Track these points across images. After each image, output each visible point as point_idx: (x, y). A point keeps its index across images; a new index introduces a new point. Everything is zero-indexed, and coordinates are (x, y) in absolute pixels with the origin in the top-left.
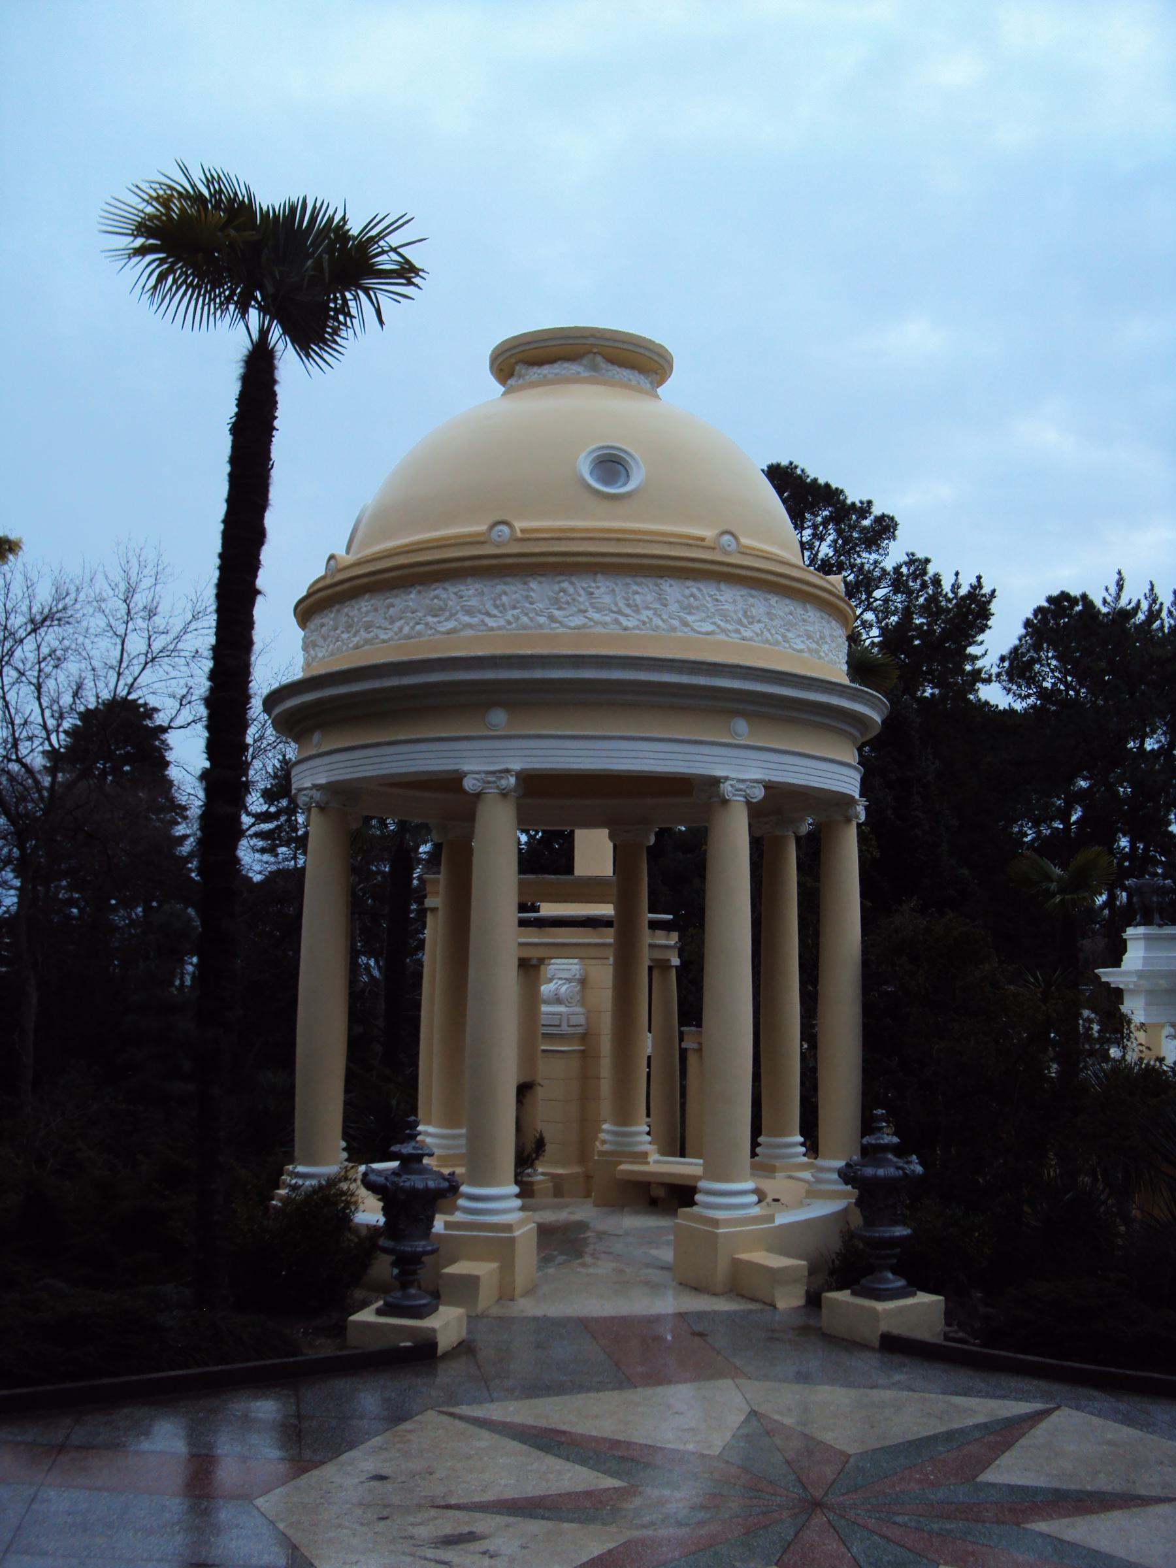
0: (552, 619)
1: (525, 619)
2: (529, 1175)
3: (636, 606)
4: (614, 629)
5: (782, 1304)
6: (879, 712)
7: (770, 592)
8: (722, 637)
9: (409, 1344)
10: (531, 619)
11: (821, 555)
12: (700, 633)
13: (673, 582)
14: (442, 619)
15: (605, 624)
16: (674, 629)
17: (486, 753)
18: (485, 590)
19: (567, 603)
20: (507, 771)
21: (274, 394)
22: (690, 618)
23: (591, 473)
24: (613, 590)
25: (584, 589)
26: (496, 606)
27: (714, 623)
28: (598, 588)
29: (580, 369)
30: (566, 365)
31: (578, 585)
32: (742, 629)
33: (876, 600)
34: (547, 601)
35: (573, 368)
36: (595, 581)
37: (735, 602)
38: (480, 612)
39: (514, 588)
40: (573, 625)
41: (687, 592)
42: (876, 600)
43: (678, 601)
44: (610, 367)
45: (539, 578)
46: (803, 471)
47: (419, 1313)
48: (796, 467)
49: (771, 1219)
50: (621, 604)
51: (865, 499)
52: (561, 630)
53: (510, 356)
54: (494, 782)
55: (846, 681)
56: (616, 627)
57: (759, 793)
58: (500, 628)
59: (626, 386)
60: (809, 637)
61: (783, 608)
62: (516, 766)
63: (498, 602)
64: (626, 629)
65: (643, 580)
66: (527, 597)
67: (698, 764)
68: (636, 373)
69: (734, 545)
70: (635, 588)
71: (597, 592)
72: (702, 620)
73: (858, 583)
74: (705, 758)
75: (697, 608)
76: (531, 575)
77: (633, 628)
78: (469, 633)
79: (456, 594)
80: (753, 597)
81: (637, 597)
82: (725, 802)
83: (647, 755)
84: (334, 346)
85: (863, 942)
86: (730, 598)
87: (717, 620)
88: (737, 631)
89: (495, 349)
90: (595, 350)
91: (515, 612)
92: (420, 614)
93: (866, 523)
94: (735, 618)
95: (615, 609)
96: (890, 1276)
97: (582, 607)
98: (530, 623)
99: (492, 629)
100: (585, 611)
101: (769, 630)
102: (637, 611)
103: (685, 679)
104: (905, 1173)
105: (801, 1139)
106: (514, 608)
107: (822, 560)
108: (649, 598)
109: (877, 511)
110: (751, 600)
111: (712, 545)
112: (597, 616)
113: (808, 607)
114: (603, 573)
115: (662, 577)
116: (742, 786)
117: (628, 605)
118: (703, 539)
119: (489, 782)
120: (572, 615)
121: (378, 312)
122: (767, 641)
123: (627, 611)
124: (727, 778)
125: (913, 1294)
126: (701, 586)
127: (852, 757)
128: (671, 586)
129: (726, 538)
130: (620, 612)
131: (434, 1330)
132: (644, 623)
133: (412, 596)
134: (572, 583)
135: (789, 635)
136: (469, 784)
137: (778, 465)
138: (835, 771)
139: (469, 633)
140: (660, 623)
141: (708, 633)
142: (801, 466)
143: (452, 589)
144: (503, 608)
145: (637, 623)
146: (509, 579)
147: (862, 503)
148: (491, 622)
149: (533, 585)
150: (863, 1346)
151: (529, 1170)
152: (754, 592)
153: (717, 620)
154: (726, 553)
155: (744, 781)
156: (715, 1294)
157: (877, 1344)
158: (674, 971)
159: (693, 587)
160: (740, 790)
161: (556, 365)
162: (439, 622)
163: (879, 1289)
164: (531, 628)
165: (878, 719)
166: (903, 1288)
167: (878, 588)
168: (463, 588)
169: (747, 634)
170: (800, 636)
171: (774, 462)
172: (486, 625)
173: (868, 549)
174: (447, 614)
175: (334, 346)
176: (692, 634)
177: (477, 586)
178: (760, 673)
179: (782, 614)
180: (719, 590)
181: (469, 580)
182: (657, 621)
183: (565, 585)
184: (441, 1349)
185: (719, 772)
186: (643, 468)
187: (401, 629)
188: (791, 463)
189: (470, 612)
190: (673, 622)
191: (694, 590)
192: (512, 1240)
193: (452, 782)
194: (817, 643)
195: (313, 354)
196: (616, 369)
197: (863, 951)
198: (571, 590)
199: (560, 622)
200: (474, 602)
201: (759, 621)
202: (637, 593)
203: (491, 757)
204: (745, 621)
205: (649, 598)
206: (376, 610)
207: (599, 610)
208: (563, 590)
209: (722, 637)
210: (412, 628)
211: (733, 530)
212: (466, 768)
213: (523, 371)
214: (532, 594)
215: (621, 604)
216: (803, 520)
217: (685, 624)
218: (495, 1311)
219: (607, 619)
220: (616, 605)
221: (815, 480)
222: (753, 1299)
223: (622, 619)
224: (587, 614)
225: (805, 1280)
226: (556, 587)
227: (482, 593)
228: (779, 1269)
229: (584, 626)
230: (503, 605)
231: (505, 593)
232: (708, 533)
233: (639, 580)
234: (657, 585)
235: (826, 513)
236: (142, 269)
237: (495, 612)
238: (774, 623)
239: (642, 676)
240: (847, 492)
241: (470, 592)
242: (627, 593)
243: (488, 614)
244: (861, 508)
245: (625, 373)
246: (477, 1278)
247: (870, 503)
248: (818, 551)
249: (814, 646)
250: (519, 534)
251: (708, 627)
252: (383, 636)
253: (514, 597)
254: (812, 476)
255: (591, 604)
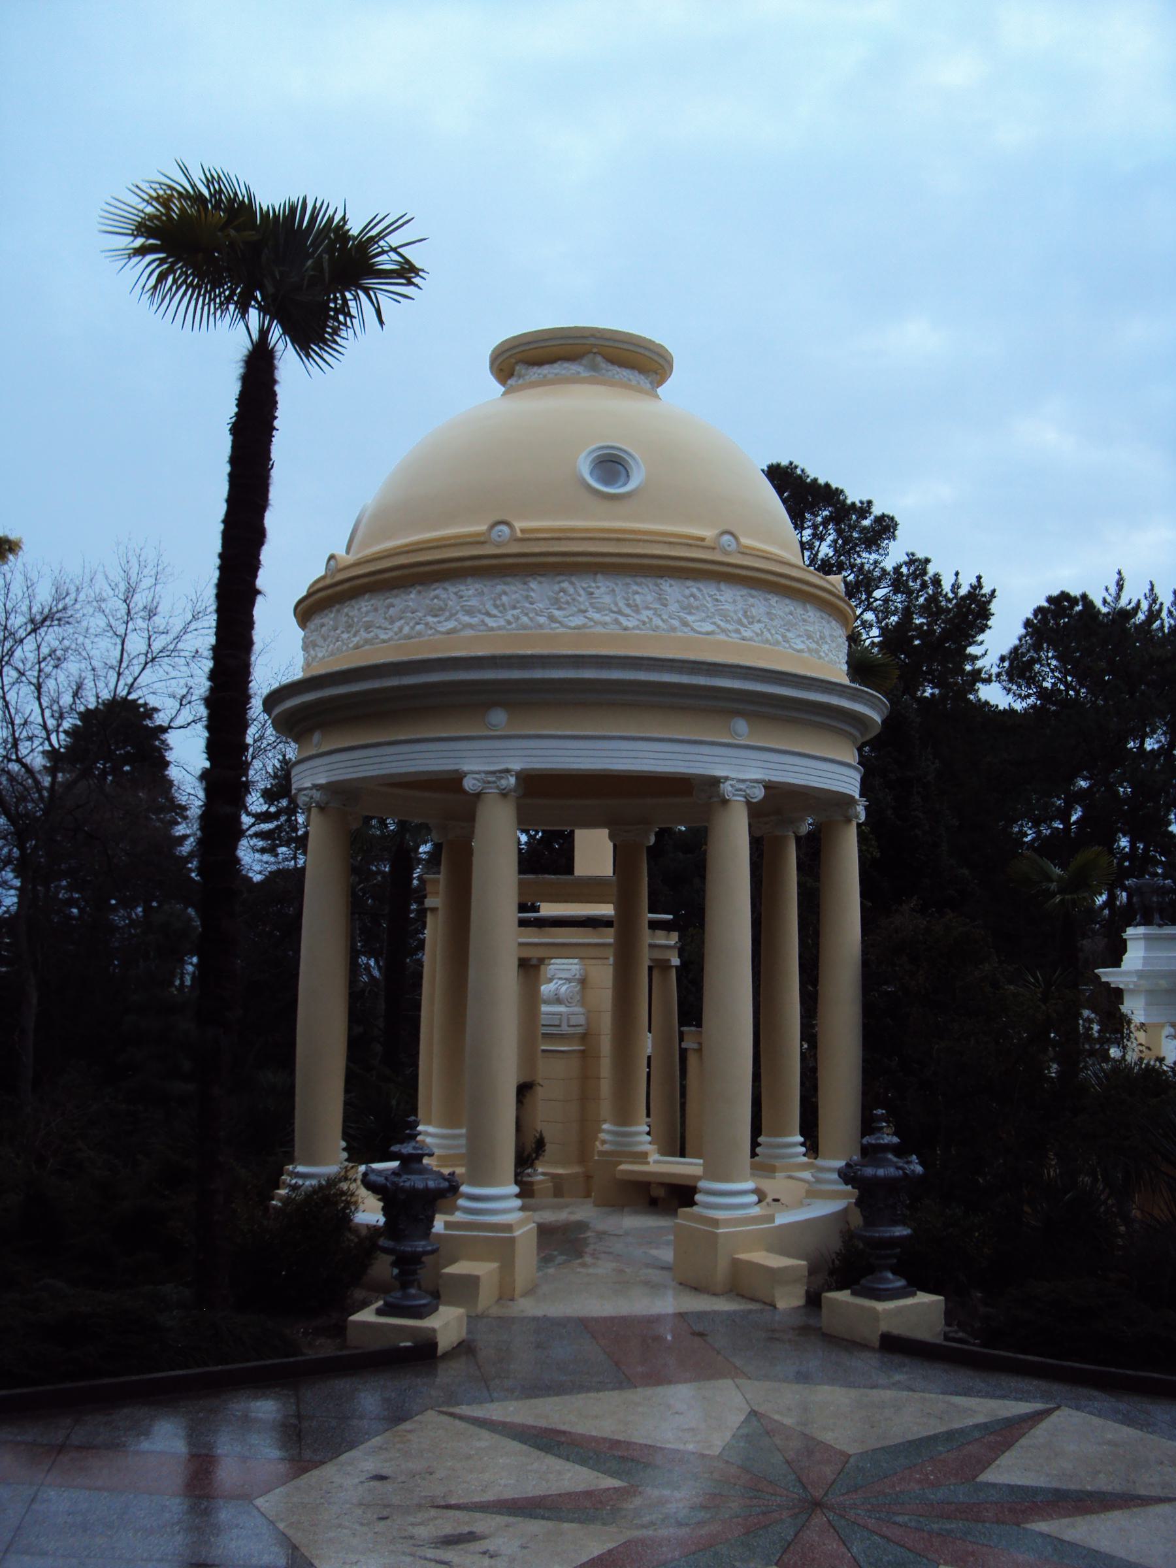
0: (552, 619)
1: (525, 619)
2: (529, 1175)
3: (636, 606)
4: (614, 629)
5: (782, 1304)
6: (879, 712)
7: (770, 592)
8: (722, 637)
9: (409, 1344)
10: (531, 619)
11: (821, 555)
12: (700, 633)
13: (673, 582)
14: (442, 619)
15: (605, 624)
16: (674, 629)
17: (486, 753)
18: (485, 590)
19: (567, 603)
20: (507, 771)
21: (274, 394)
22: (690, 618)
23: (591, 473)
24: (613, 590)
25: (584, 589)
26: (496, 606)
27: (714, 623)
28: (598, 588)
29: (580, 369)
30: (566, 365)
31: (578, 585)
32: (742, 629)
33: (876, 600)
34: (547, 601)
35: (573, 368)
36: (595, 581)
37: (735, 602)
38: (480, 612)
39: (514, 588)
40: (573, 625)
41: (687, 592)
42: (876, 600)
43: (678, 601)
44: (610, 367)
45: (539, 578)
46: (803, 471)
47: (419, 1313)
48: (796, 467)
49: (771, 1219)
50: (621, 604)
51: (865, 499)
52: (561, 630)
53: (510, 356)
54: (494, 782)
55: (846, 681)
56: (616, 627)
57: (759, 793)
58: (500, 628)
59: (626, 386)
60: (809, 637)
61: (783, 608)
62: (516, 766)
63: (498, 602)
64: (626, 629)
65: (643, 580)
66: (527, 597)
67: (698, 764)
68: (636, 373)
69: (734, 545)
70: (635, 588)
71: (597, 592)
72: (702, 620)
73: (858, 583)
74: (705, 758)
75: (697, 608)
76: (531, 575)
77: (633, 628)
78: (469, 633)
79: (456, 594)
80: (753, 597)
81: (637, 597)
82: (725, 802)
83: (647, 755)
84: (334, 346)
85: (863, 942)
86: (730, 598)
87: (717, 620)
88: (737, 631)
89: (495, 349)
90: (595, 350)
91: (515, 612)
92: (420, 614)
93: (866, 523)
94: (735, 618)
95: (615, 609)
96: (890, 1276)
97: (582, 607)
98: (530, 623)
99: (492, 629)
100: (585, 611)
101: (769, 630)
102: (637, 611)
103: (685, 679)
104: (905, 1173)
105: (801, 1139)
106: (514, 608)
107: (822, 560)
108: (649, 598)
109: (877, 511)
110: (751, 600)
111: (712, 545)
112: (597, 616)
113: (808, 607)
114: (603, 573)
115: (662, 577)
116: (742, 786)
117: (628, 605)
118: (703, 539)
119: (489, 782)
120: (572, 615)
121: (378, 312)
122: (767, 641)
123: (627, 611)
124: (727, 778)
125: (913, 1294)
126: (701, 586)
127: (852, 757)
128: (671, 586)
129: (726, 538)
130: (620, 612)
131: (434, 1330)
132: (644, 623)
133: (412, 596)
134: (572, 583)
135: (789, 635)
136: (469, 784)
137: (778, 465)
138: (835, 771)
139: (469, 633)
140: (660, 623)
141: (708, 633)
142: (801, 466)
143: (452, 589)
144: (503, 608)
145: (637, 623)
146: (509, 579)
147: (862, 503)
148: (491, 622)
149: (533, 585)
150: (863, 1346)
151: (529, 1170)
152: (754, 592)
153: (717, 620)
154: (726, 553)
155: (744, 781)
156: (715, 1294)
157: (877, 1344)
158: (674, 971)
159: (693, 587)
160: (740, 790)
161: (556, 365)
162: (439, 622)
163: (879, 1289)
164: (531, 628)
165: (878, 719)
166: (903, 1288)
167: (878, 588)
168: (463, 588)
169: (747, 634)
170: (800, 636)
171: (774, 462)
172: (486, 625)
173: (868, 549)
174: (447, 614)
175: (334, 346)
176: (692, 634)
177: (477, 586)
178: (760, 673)
179: (782, 614)
180: (719, 590)
181: (469, 580)
182: (657, 621)
183: (565, 585)
184: (441, 1349)
185: (719, 772)
186: (643, 468)
187: (401, 629)
188: (791, 463)
189: (470, 612)
190: (673, 622)
191: (694, 590)
192: (512, 1240)
193: (452, 782)
194: (817, 643)
195: (313, 354)
196: (616, 369)
197: (863, 951)
198: (571, 590)
199: (560, 622)
200: (474, 602)
201: (759, 621)
202: (637, 593)
203: (491, 757)
204: (745, 621)
205: (649, 598)
206: (376, 610)
207: (599, 610)
208: (563, 590)
209: (722, 637)
210: (412, 628)
211: (733, 530)
212: (466, 768)
213: (523, 371)
214: (532, 594)
215: (621, 604)
216: (803, 520)
217: (685, 624)
218: (495, 1311)
219: (607, 619)
220: (616, 605)
221: (815, 480)
222: (753, 1299)
223: (622, 619)
224: (587, 614)
225: (805, 1280)
226: (556, 587)
227: (482, 593)
228: (779, 1269)
229: (584, 626)
230: (503, 605)
231: (505, 593)
232: (708, 533)
233: (639, 580)
234: (657, 585)
235: (826, 513)
236: (142, 269)
237: (495, 612)
238: (774, 623)
239: (642, 676)
240: (847, 492)
241: (470, 592)
242: (627, 593)
243: (488, 614)
244: (861, 508)
245: (625, 373)
246: (477, 1278)
247: (870, 503)
248: (818, 551)
249: (814, 646)
250: (519, 534)
251: (708, 627)
252: (383, 636)
253: (514, 597)
254: (812, 476)
255: (591, 604)
